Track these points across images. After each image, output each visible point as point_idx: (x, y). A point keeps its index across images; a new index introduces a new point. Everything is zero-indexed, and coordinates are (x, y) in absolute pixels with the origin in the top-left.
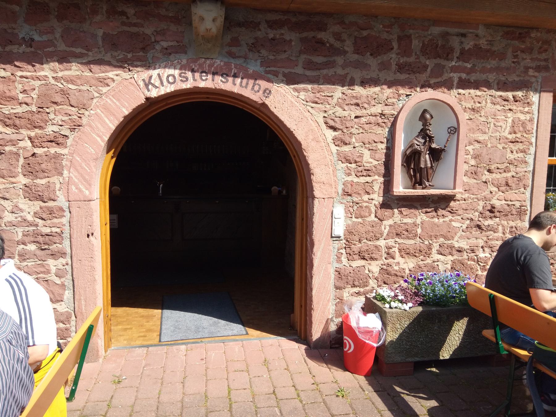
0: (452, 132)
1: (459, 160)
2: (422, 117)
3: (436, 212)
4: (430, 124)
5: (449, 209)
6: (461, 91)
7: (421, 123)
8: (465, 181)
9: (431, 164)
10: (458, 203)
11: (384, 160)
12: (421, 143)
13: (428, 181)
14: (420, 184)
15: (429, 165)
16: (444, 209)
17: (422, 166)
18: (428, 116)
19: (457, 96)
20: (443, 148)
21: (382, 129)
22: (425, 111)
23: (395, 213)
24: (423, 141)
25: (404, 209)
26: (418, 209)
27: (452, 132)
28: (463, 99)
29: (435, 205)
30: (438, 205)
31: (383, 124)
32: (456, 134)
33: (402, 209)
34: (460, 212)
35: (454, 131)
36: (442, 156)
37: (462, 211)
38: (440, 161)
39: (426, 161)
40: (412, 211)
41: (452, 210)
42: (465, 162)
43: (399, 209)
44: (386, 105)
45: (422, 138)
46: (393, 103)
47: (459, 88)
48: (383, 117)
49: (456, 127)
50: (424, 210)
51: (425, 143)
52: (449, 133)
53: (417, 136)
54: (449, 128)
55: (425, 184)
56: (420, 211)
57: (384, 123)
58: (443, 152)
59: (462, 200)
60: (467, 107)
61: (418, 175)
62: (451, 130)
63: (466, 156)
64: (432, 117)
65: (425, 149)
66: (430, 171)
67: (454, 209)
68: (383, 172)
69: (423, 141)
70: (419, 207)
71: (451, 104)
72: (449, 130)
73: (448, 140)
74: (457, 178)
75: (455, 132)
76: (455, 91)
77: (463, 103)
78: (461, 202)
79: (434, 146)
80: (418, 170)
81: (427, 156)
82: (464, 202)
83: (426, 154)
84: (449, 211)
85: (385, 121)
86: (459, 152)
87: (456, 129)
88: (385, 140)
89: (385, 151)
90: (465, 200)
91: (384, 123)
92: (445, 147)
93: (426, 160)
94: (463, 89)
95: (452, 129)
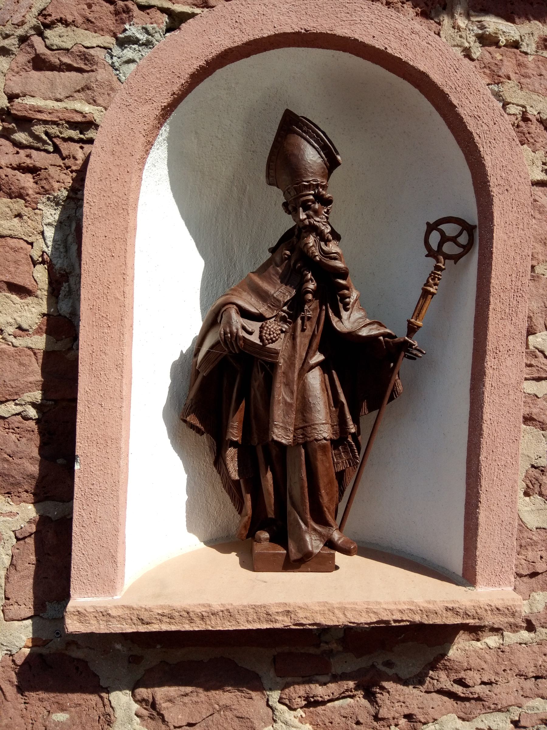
0: (448, 248)
1: (489, 412)
2: (281, 165)
3: (370, 696)
4: (326, 202)
5: (444, 680)
6: (494, 24)
7: (277, 196)
8: (532, 521)
9: (341, 424)
10: (492, 640)
11: (37, 395)
12: (274, 303)
13: (320, 518)
14: (280, 537)
15: (324, 431)
16: (418, 680)
17: (281, 435)
18: (311, 156)
19: (477, 51)
20: (402, 334)
21: (19, 205)
22: (292, 124)
23: (119, 714)
24: (284, 294)
25: (172, 691)
26: (259, 687)
27: (448, 248)
28: (508, 67)
29: (363, 662)
30: (378, 660)
31: (27, 181)
32: (474, 257)
33: (161, 693)
34: (507, 690)
35: (463, 239)
36: (399, 383)
37: (514, 682)
38: (386, 407)
39: (304, 407)
40: (227, 697)
41: (460, 682)
42: (528, 419)
43: (143, 692)
44: (39, 64)
45: (286, 279)
46: (85, 58)
47: (485, 11)
48: (21, 137)
49: (472, 216)
50: (298, 691)
51: (296, 306)
52: (431, 253)
53: (262, 271)
54: (431, 227)
55: (301, 543)
56: (275, 696)
57: (33, 170)
58: (404, 363)
59: (515, 628)
60: (532, 112)
61: (268, 480)
62: (444, 239)
63: (531, 387)
64: (332, 162)
65: (302, 341)
66: (327, 465)
67: (472, 677)
68: (34, 469)
69: (284, 294)
70: (268, 674)
71: (436, 77)
72: (435, 238)
73: (426, 294)
74: (483, 516)
75: (467, 248)
76: (462, 22)
77: (509, 90)
78: (511, 638)
79: (350, 321)
80: (260, 453)
81: (315, 378)
82: (525, 635)
83: (306, 368)
84: (440, 692)
85: (39, 159)
86: (490, 362)
87: (469, 228)
88: (41, 274)
89: (39, 342)
90: (530, 627)
91: (33, 170)
92: (412, 329)
93: (309, 397)
94: (510, 19)
95: (450, 229)
